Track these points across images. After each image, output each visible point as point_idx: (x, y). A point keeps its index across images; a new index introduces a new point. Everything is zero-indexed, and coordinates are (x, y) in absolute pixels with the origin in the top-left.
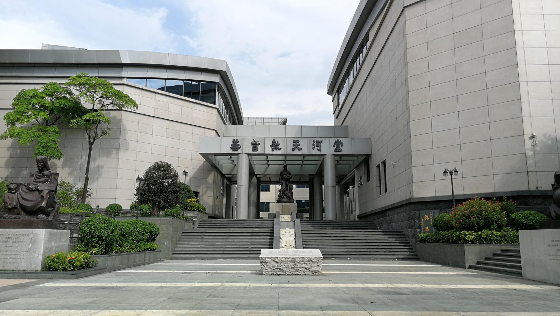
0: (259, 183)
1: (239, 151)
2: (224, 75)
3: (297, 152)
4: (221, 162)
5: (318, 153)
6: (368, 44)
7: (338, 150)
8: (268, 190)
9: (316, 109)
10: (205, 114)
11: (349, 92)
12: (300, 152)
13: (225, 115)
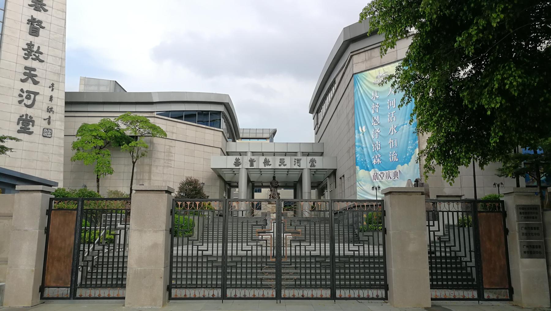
0: (254, 186)
1: (240, 167)
2: (228, 106)
3: (282, 167)
4: (225, 172)
5: (298, 168)
6: (336, 86)
7: (313, 165)
8: (260, 191)
9: (297, 129)
10: (213, 136)
11: (325, 115)
12: (285, 167)
13: (227, 135)
